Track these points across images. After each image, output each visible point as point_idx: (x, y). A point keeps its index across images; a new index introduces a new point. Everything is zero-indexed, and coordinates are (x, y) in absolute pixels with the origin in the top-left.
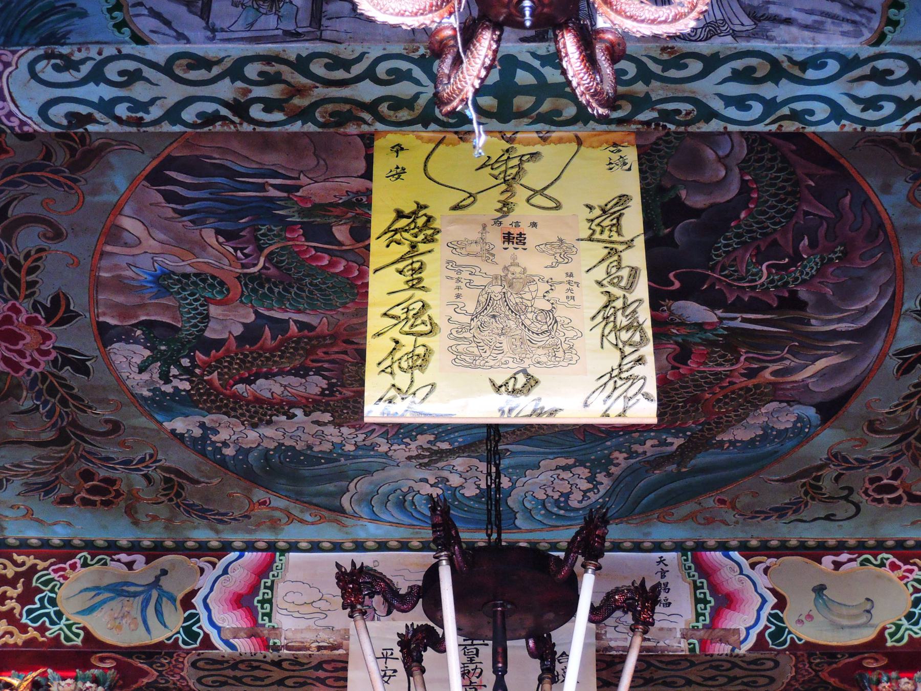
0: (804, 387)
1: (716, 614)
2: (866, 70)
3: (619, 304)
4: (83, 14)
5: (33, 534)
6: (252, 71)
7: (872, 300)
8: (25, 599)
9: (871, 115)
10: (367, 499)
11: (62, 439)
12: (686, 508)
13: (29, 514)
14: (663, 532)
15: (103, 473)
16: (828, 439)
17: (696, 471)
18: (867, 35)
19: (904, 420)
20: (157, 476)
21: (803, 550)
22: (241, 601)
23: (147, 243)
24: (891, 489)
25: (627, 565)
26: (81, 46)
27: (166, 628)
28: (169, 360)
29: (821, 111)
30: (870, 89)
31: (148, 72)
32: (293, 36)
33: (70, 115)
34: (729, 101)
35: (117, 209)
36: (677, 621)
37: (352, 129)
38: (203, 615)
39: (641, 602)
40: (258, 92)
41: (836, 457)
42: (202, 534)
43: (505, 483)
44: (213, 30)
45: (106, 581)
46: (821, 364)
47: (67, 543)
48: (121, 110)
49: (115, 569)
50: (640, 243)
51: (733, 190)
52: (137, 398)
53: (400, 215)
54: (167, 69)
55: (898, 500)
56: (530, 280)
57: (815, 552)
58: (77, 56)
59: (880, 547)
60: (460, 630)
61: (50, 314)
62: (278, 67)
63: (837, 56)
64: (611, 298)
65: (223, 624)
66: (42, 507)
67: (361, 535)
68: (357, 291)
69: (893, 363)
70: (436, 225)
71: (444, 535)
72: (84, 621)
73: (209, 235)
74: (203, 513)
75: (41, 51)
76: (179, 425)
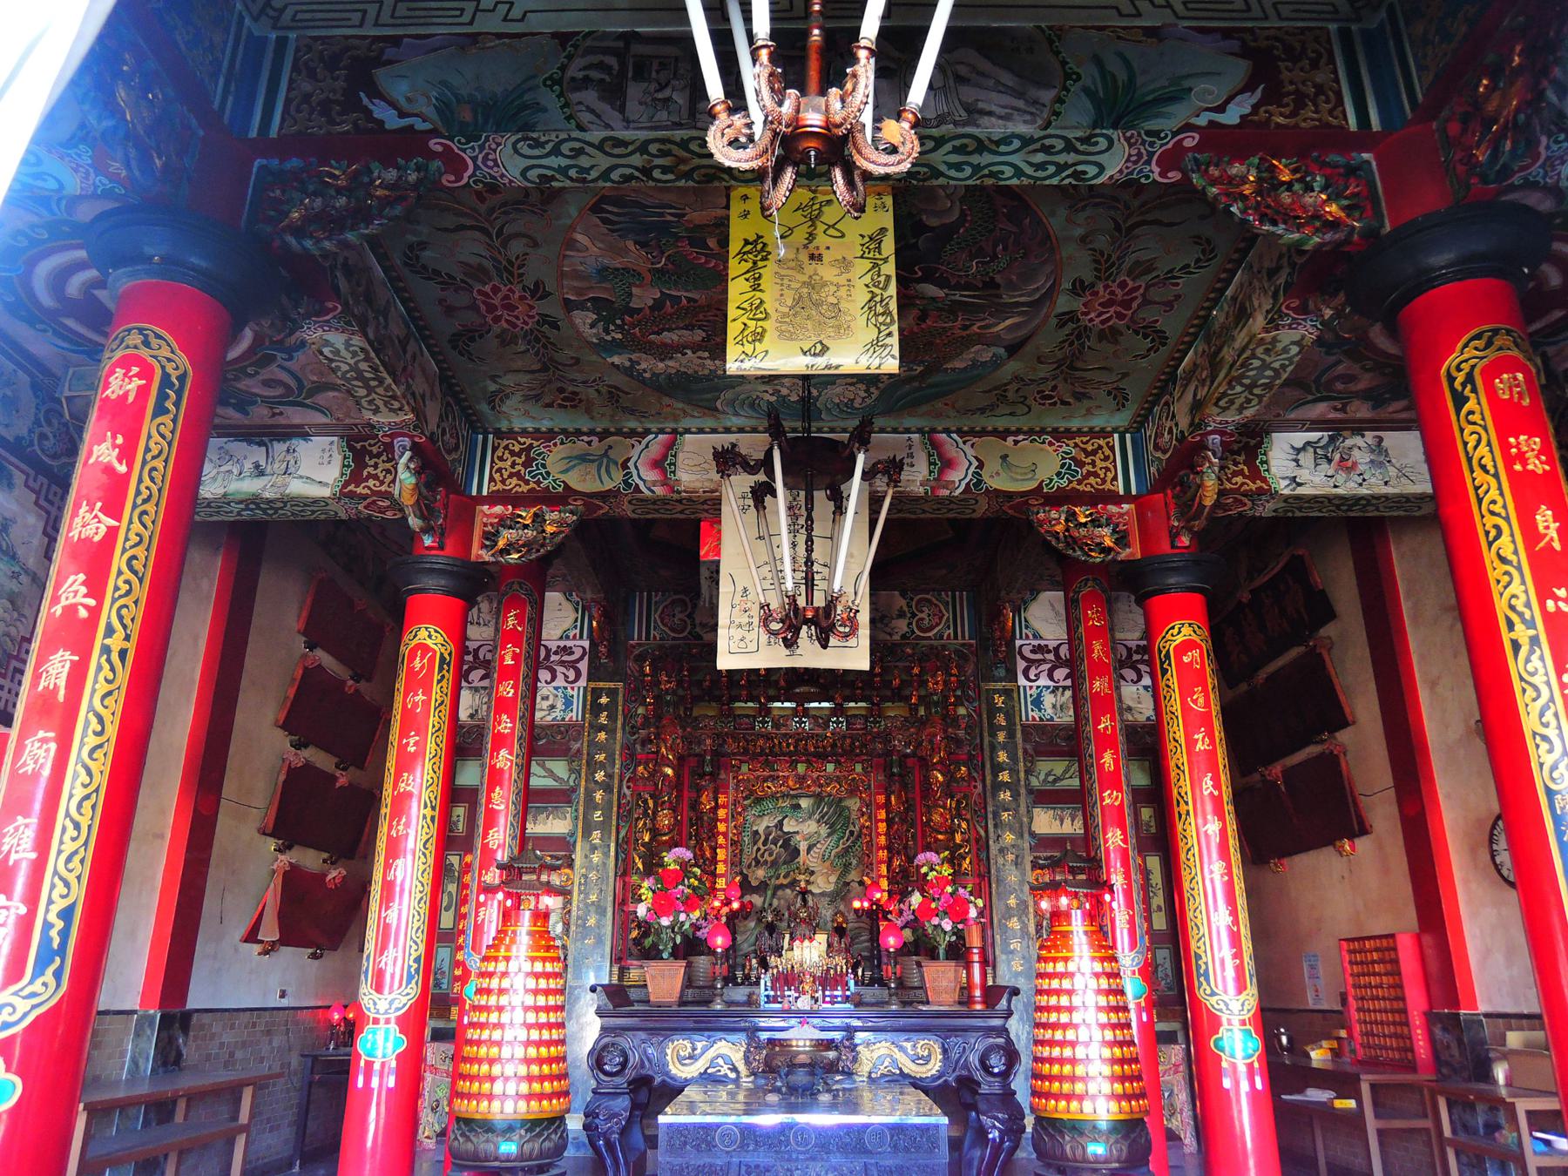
0: (998, 335)
1: (941, 472)
2: (1037, 146)
3: (878, 299)
4: (545, 110)
5: (529, 425)
6: (653, 148)
7: (1041, 283)
8: (526, 465)
9: (1040, 174)
10: (732, 403)
11: (545, 369)
12: (924, 408)
13: (526, 413)
14: (910, 422)
15: (571, 389)
16: (1013, 367)
17: (931, 386)
18: (1040, 122)
19: (1060, 355)
20: (604, 390)
21: (995, 433)
22: (657, 464)
23: (591, 249)
24: (1051, 397)
25: (886, 442)
26: (545, 132)
27: (612, 482)
28: (609, 321)
29: (1009, 171)
30: (1040, 157)
31: (588, 149)
32: (678, 125)
33: (541, 176)
34: (950, 166)
35: (572, 228)
36: (917, 477)
37: (716, 184)
38: (635, 473)
39: (892, 468)
40: (658, 161)
41: (1016, 378)
42: (632, 424)
43: (815, 393)
44: (628, 122)
45: (575, 453)
46: (1008, 322)
47: (551, 431)
48: (573, 173)
49: (581, 445)
50: (892, 259)
51: (956, 214)
52: (590, 344)
53: (747, 242)
54: (600, 147)
55: (1054, 404)
56: (824, 284)
57: (1003, 434)
58: (543, 139)
59: (1043, 431)
60: (785, 485)
61: (533, 294)
62: (669, 146)
63: (1018, 136)
64: (874, 296)
65: (646, 478)
66: (535, 410)
67: (729, 424)
68: (722, 279)
69: (1054, 321)
70: (769, 249)
71: (776, 431)
72: (563, 477)
73: (630, 244)
74: (632, 412)
75: (519, 136)
76: (616, 360)
